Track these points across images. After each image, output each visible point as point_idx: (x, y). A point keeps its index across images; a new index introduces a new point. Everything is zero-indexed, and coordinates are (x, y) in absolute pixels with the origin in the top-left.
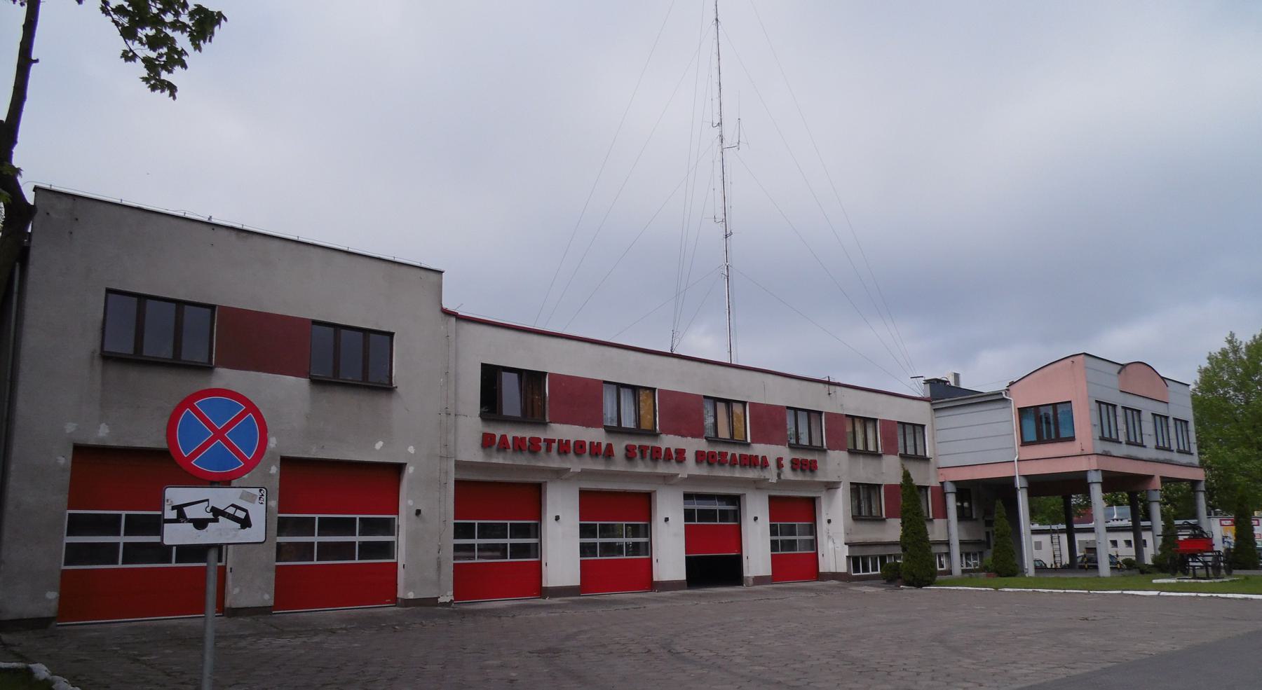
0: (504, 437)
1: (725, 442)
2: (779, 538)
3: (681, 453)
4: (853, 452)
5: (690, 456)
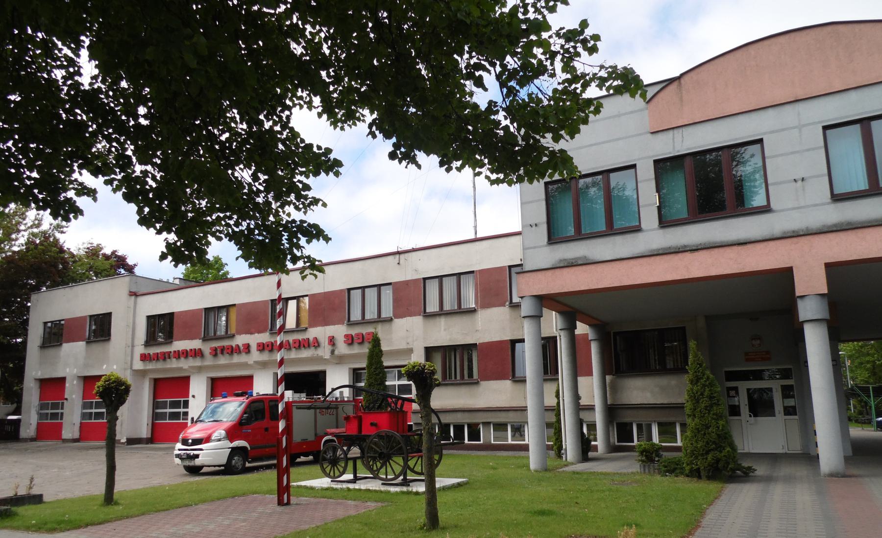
2: (182, 410)
3: (247, 348)
4: (428, 316)
5: (254, 348)
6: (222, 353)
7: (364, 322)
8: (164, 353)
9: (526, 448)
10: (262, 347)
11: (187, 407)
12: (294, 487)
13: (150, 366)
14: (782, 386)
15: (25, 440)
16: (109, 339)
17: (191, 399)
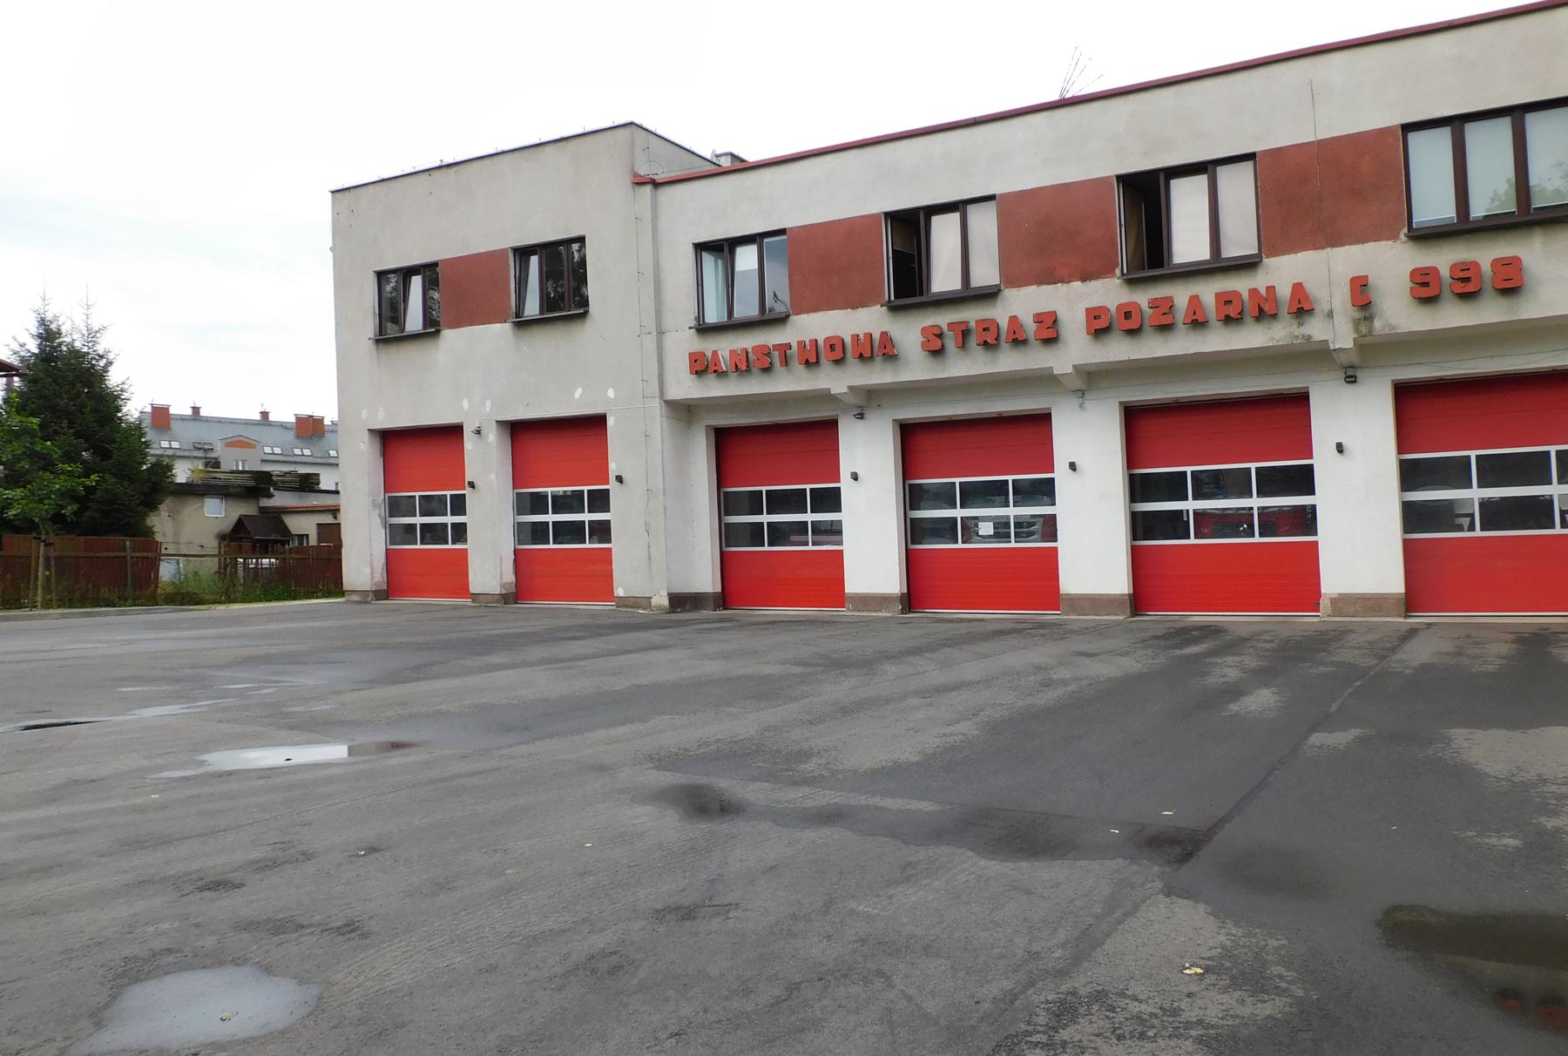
0: (1194, 300)
1: (1496, 226)
2: (449, 519)
3: (1049, 331)
6: (786, 361)
7: (1464, 228)
8: (765, 351)
10: (1099, 325)
13: (715, 389)
15: (633, 619)
16: (584, 315)
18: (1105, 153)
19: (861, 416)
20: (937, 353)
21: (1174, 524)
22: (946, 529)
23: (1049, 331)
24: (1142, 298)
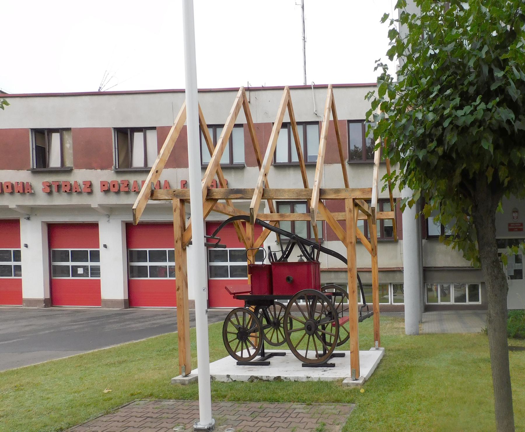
2: (13, 263)
3: (89, 189)
5: (97, 188)
9: (401, 309)
11: (19, 260)
12: (267, 353)
14: (20, 261)
17: (23, 249)
18: (107, 118)
19: (28, 219)
20: (50, 193)
21: (142, 271)
22: (65, 271)
23: (89, 189)
24: (119, 179)
